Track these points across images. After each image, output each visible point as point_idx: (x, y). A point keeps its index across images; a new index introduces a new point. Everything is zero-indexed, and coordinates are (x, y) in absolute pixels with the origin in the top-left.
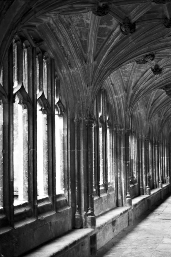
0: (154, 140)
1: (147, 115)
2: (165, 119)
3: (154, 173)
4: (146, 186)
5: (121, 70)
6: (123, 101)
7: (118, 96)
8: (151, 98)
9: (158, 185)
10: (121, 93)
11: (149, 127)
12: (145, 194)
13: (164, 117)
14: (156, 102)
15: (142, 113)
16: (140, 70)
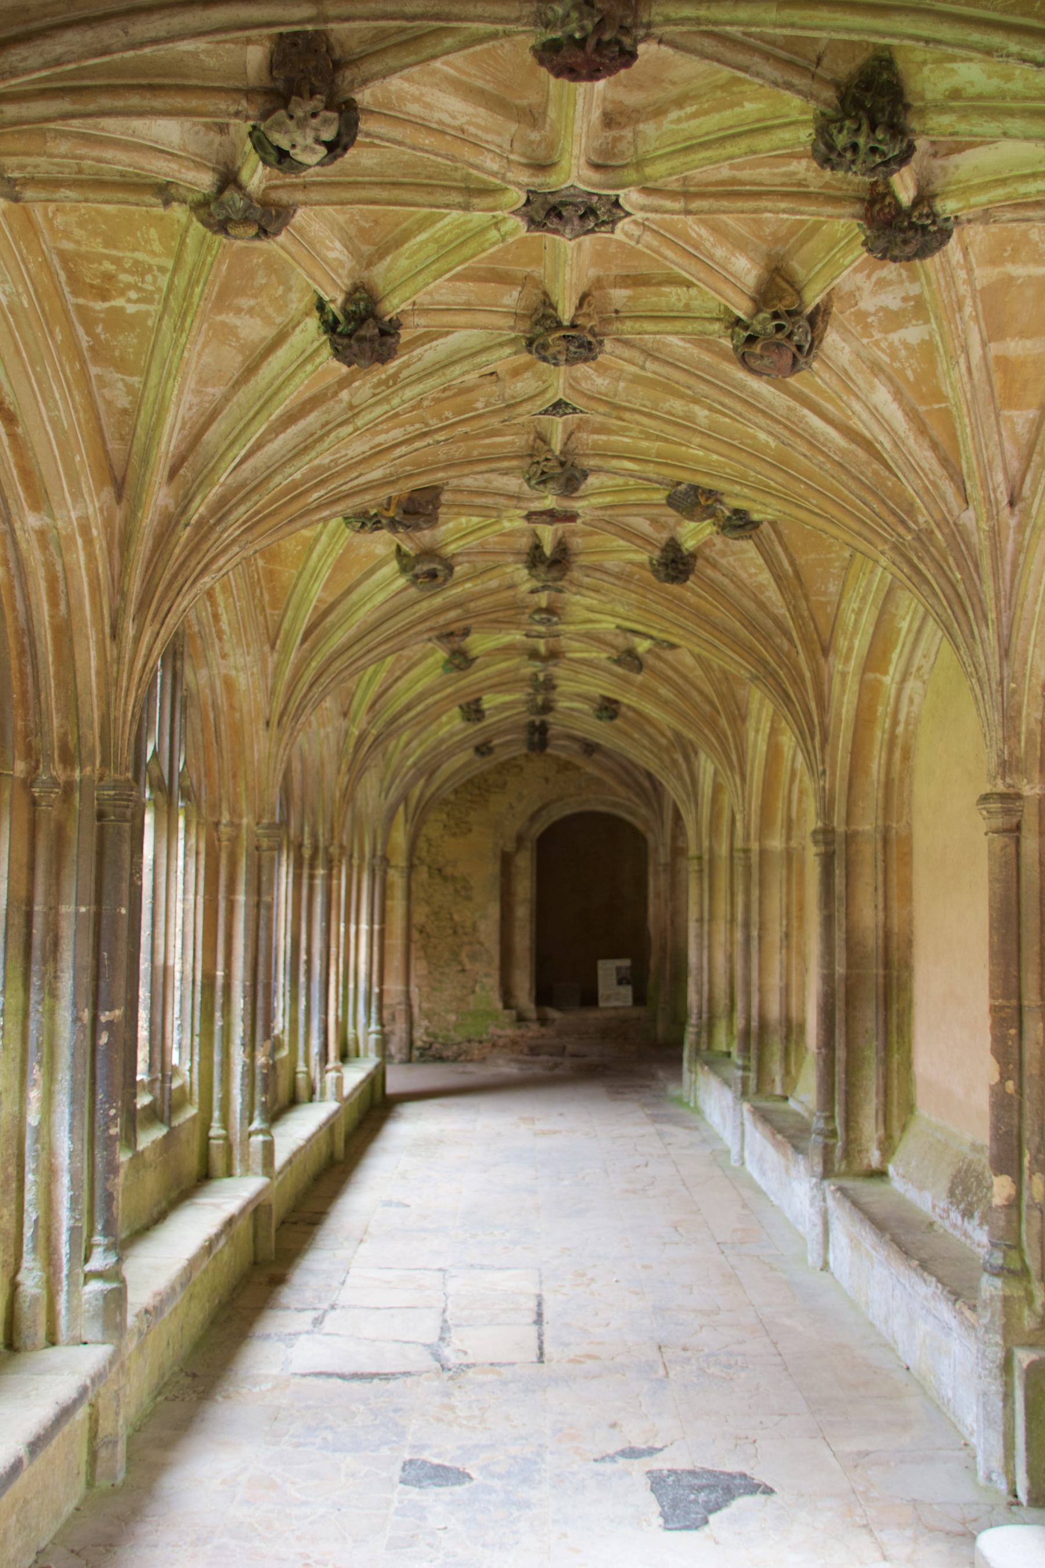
0: (307, 842)
1: (272, 693)
2: (374, 732)
3: (302, 1017)
4: (250, 1122)
5: (81, 301)
6: (91, 558)
7: (52, 516)
8: (307, 590)
9: (318, 1086)
10: (77, 495)
11: (281, 768)
12: (238, 1169)
13: (369, 723)
14: (331, 618)
15: (242, 681)
16: (230, 318)
